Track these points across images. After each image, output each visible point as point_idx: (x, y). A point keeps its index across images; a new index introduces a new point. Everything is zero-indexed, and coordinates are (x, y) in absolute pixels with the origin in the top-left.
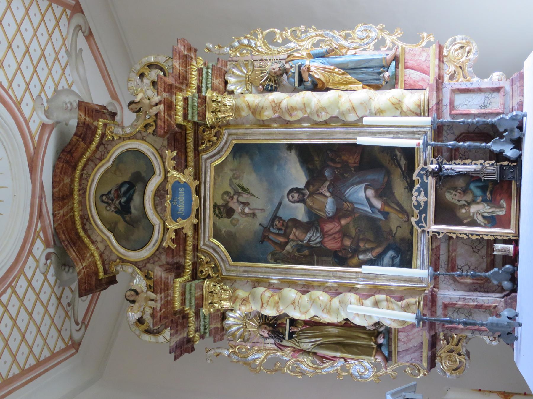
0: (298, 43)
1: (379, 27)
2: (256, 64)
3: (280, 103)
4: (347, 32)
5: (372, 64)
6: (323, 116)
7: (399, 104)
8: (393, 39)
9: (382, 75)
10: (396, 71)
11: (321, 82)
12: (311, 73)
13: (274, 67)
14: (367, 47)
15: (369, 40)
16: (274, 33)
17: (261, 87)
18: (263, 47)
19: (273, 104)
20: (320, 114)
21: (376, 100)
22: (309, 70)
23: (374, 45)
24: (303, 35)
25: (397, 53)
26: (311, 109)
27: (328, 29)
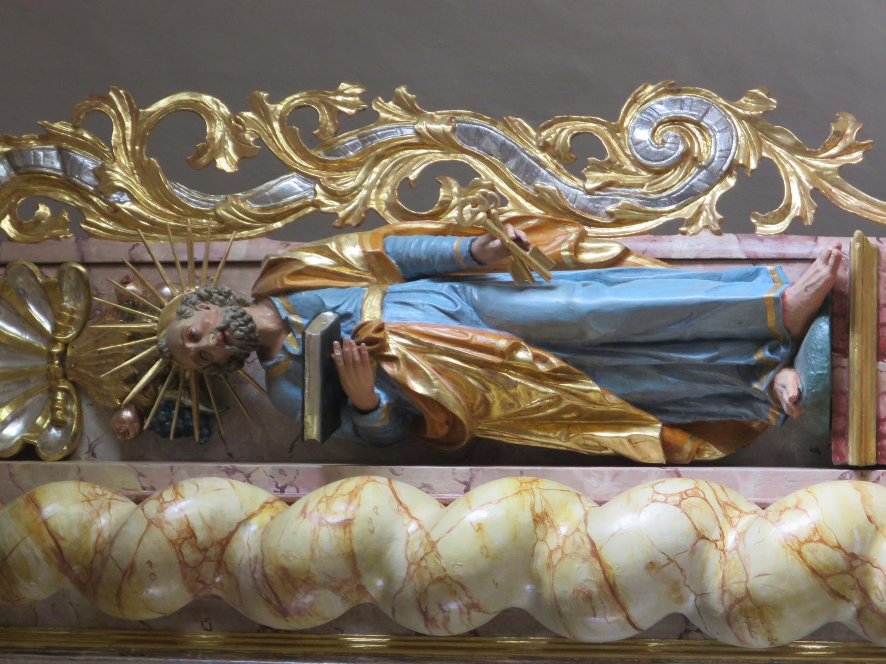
0: (323, 175)
1: (749, 106)
2: (100, 279)
3: (225, 543)
4: (580, 125)
5: (709, 326)
6: (454, 618)
7: (851, 570)
8: (820, 173)
9: (759, 386)
10: (833, 368)
11: (440, 418)
12: (387, 368)
13: (193, 323)
14: (687, 212)
15: (696, 177)
16: (197, 116)
17: (127, 414)
18: (140, 192)
19: (187, 550)
20: (434, 612)
21: (730, 539)
22: (376, 348)
23: (723, 204)
24: (349, 139)
25: (843, 273)
26: (389, 580)
27: (479, 110)
